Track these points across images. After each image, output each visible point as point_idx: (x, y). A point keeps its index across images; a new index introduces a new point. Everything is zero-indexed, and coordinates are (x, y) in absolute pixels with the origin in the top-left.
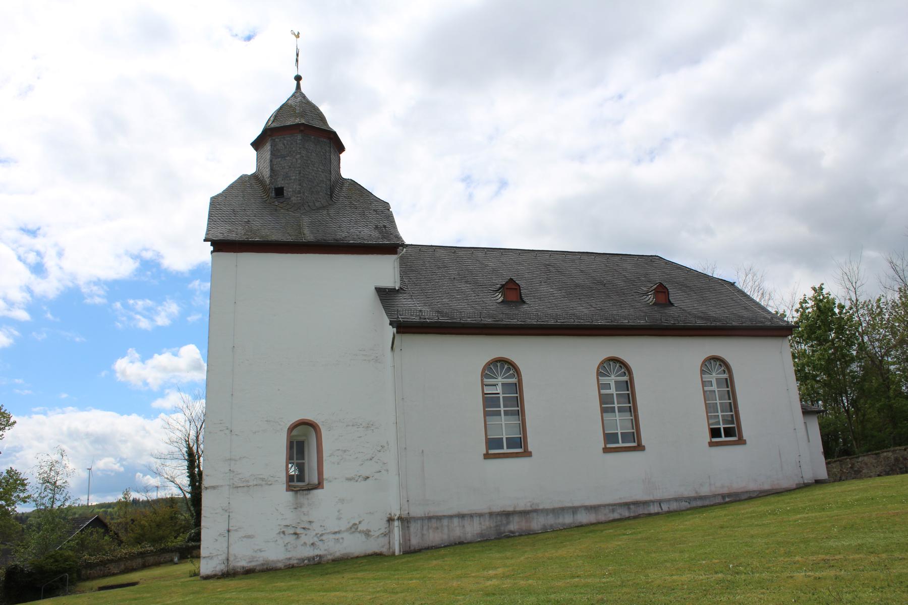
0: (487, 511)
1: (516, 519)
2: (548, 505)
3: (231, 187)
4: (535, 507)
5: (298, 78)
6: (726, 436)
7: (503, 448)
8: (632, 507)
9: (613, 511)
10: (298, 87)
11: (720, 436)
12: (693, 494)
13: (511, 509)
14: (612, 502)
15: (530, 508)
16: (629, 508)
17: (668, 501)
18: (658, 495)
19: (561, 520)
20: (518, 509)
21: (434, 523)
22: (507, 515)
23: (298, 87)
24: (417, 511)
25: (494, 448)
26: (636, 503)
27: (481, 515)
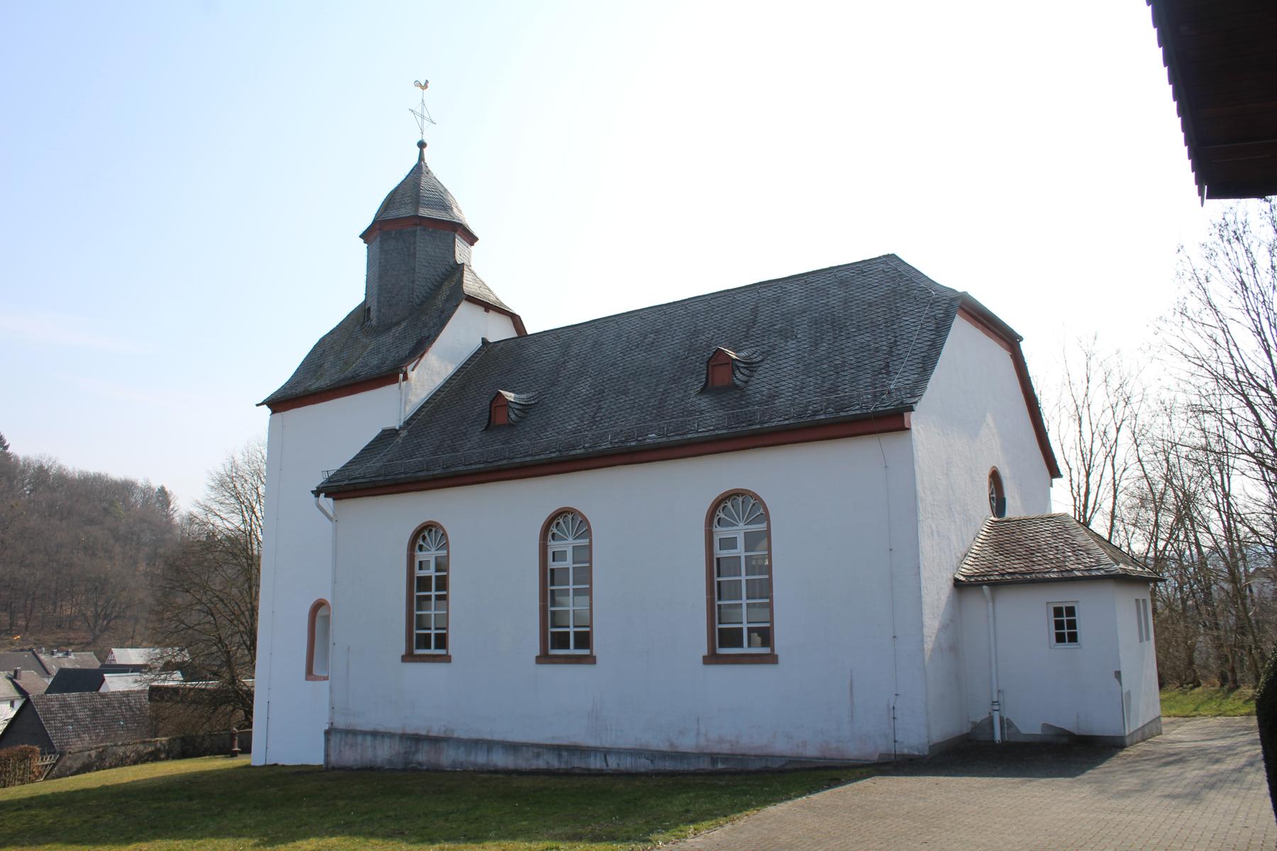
0: (400, 731)
1: (425, 747)
2: (464, 735)
3: (332, 332)
4: (449, 734)
5: (422, 145)
6: (576, 647)
8: (565, 754)
9: (538, 756)
10: (421, 158)
11: (429, 647)
12: (664, 747)
13: (423, 732)
14: (541, 741)
15: (442, 735)
16: (560, 756)
17: (619, 752)
18: (608, 741)
19: (472, 758)
20: (433, 734)
21: (350, 739)
22: (417, 739)
23: (421, 158)
24: (341, 723)
25: (1071, 611)
26: (574, 749)
27: (391, 735)
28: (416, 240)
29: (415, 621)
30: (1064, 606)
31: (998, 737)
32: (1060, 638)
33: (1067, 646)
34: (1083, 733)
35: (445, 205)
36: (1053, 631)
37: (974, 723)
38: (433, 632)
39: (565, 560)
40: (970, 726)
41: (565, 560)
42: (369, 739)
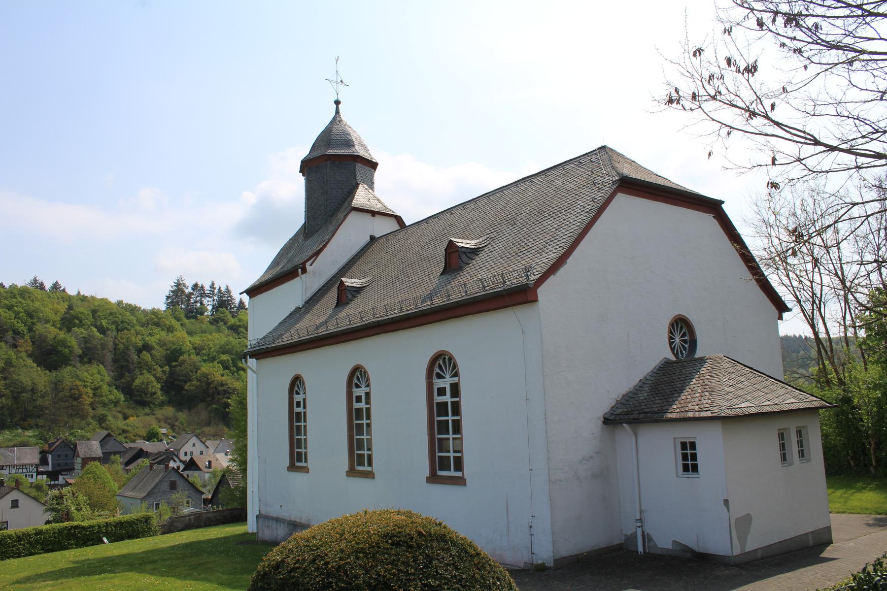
5: (337, 103)
7: (364, 465)
10: (337, 112)
23: (337, 112)
24: (263, 512)
25: (693, 445)
28: (335, 169)
29: (436, 445)
30: (688, 441)
31: (640, 549)
32: (686, 469)
33: (690, 474)
34: (701, 551)
35: (349, 144)
36: (680, 462)
37: (626, 535)
38: (452, 455)
39: (445, 395)
40: (623, 538)
41: (445, 395)
42: (274, 522)
